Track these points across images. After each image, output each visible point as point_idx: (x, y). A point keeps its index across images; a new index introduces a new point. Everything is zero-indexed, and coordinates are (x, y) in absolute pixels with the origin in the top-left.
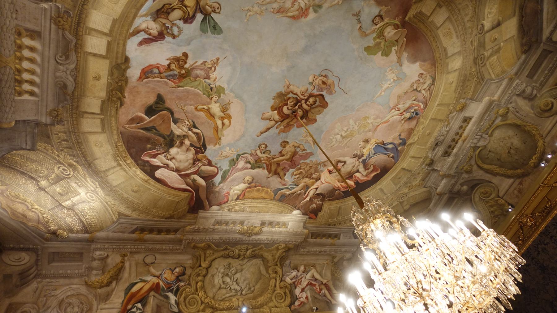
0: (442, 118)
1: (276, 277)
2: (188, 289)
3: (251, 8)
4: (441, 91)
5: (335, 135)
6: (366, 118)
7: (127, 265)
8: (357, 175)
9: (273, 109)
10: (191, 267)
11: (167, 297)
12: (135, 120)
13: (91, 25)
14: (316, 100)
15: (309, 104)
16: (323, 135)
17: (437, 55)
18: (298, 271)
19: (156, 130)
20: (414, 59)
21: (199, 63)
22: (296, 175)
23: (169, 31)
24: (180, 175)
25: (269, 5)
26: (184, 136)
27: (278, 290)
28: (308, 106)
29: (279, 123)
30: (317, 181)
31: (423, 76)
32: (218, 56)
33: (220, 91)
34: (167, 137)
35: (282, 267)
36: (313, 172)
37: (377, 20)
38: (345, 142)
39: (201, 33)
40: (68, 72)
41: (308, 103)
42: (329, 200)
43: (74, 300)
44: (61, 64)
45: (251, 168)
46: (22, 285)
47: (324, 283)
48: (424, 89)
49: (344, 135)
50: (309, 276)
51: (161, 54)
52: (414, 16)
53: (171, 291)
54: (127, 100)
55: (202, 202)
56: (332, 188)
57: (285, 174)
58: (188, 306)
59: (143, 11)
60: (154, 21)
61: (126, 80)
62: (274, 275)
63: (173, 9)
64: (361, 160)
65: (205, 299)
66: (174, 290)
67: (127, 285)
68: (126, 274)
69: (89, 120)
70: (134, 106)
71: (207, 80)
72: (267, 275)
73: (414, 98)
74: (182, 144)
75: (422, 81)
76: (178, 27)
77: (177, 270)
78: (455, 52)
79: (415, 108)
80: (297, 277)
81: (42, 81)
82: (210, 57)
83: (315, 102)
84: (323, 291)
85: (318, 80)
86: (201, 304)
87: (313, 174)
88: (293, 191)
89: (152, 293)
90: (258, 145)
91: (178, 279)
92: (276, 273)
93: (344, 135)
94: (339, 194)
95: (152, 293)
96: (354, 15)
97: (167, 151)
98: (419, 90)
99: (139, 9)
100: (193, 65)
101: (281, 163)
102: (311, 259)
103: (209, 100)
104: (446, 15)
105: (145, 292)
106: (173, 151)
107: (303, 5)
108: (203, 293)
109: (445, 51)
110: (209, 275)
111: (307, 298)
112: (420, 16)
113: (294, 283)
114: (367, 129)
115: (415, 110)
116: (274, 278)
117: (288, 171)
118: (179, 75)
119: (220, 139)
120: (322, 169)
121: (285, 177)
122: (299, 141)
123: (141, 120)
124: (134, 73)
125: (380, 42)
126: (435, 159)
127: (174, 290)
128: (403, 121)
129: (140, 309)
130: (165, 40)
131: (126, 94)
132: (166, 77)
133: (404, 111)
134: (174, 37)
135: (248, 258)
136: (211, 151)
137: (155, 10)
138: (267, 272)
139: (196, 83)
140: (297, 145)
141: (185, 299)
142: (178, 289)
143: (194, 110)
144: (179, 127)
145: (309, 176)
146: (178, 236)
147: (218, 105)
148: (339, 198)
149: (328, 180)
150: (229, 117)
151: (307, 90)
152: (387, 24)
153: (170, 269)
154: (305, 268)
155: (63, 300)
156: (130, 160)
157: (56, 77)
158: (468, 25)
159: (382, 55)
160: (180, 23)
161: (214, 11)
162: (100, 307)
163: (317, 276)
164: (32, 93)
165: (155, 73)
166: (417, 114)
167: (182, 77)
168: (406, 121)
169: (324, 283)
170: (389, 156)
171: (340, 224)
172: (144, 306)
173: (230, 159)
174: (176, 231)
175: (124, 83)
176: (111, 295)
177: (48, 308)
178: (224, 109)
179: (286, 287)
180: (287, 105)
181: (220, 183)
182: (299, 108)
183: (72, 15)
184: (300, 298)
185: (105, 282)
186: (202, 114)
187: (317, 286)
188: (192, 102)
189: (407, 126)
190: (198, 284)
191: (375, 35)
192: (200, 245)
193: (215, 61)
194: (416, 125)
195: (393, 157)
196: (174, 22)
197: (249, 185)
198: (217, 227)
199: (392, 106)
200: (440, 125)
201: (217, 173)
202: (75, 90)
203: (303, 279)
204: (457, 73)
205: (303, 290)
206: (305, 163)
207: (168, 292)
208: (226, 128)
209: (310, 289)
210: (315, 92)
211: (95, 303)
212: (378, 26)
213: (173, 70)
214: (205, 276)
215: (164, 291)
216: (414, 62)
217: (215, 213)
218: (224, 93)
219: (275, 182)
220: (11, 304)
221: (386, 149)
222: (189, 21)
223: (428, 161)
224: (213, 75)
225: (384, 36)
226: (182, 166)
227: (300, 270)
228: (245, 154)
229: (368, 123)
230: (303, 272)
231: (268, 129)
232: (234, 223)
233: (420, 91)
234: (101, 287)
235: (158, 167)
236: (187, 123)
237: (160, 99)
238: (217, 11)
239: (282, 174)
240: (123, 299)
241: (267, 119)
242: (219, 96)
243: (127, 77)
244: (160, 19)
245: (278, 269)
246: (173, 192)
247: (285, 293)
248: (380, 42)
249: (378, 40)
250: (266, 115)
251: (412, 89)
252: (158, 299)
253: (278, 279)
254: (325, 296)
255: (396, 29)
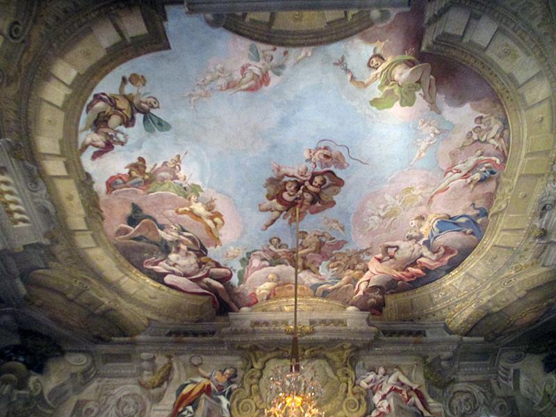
0: (541, 171)
1: (347, 380)
2: (241, 393)
3: (192, 93)
4: (526, 135)
5: (369, 216)
6: (408, 190)
7: (175, 365)
8: (422, 260)
9: (270, 198)
10: (242, 369)
11: (219, 401)
12: (122, 232)
13: (43, 150)
14: (325, 179)
15: (317, 184)
16: (351, 219)
17: (498, 87)
18: (377, 374)
19: (146, 239)
20: (459, 98)
21: (159, 165)
22: (333, 267)
23: (114, 139)
24: (191, 280)
25: (213, 83)
26: (177, 241)
27: (350, 397)
28: (317, 187)
29: (285, 212)
30: (365, 272)
31: (483, 121)
32: (177, 153)
33: (196, 189)
34: (160, 244)
35: (354, 369)
36: (355, 262)
37: (375, 62)
38: (389, 222)
39: (147, 133)
40: (44, 197)
41: (314, 183)
42: (392, 293)
43: (130, 400)
44: (36, 191)
45: (271, 265)
46: (86, 383)
47: (414, 388)
48: (493, 138)
49: (382, 214)
50: (392, 380)
51: (116, 163)
52: (434, 43)
53: (223, 394)
54: (105, 214)
55: (227, 305)
56: (390, 279)
57: (318, 268)
58: (241, 411)
59: (82, 125)
60: (96, 132)
61: (96, 195)
62: (345, 378)
63: (109, 117)
64: (421, 242)
65: (260, 404)
66: (226, 393)
67: (177, 387)
68: (175, 375)
69: (81, 237)
70: (115, 219)
71: (176, 181)
72: (336, 378)
73: (479, 152)
74: (178, 249)
75: (483, 127)
76: (122, 133)
77: (228, 371)
78: (531, 75)
79: (486, 165)
80: (376, 381)
81: (27, 209)
82: (168, 155)
83: (324, 182)
84: (412, 399)
85: (317, 154)
86: (256, 410)
87: (356, 262)
88: (336, 285)
89: (203, 395)
90: (268, 240)
91: (230, 381)
92: (347, 375)
93: (382, 214)
94: (403, 284)
95: (203, 395)
96: (335, 64)
97: (166, 258)
98: (483, 139)
99: (77, 125)
100: (153, 169)
101: (307, 256)
102: (394, 360)
103: (187, 201)
104: (493, 27)
105: (196, 395)
106: (173, 257)
107: (257, 71)
108: (258, 397)
109: (511, 77)
110: (265, 377)
111: (389, 407)
112: (445, 40)
113: (372, 388)
114: (416, 203)
115: (486, 168)
116: (345, 382)
117: (320, 264)
118: (145, 182)
119: (218, 239)
120: (366, 258)
121: (320, 271)
122: (321, 229)
123: (127, 231)
124: (100, 186)
125: (393, 90)
126: (549, 228)
127: (226, 393)
128: (472, 186)
129: (191, 413)
130: (115, 149)
131: (102, 209)
132: (133, 185)
133: (469, 172)
134: (123, 144)
135: (307, 358)
136: (212, 252)
137: (92, 121)
138: (335, 374)
139: (166, 186)
140: (320, 234)
141: (238, 403)
142: (230, 392)
143: (176, 214)
144: (167, 233)
145: (352, 267)
146: (216, 338)
147: (200, 204)
148: (403, 289)
149: (380, 270)
150: (219, 215)
151: (307, 169)
152: (392, 63)
153: (220, 370)
154: (386, 370)
155: (120, 400)
156: (135, 270)
157: (35, 203)
158: (542, 30)
159: (402, 105)
160: (122, 128)
161: (152, 107)
162: (153, 408)
163: (404, 380)
164: (24, 221)
165: (120, 184)
166: (492, 173)
167: (147, 182)
168: (476, 184)
169: (414, 388)
170: (465, 232)
171: (419, 318)
172: (195, 409)
173: (239, 258)
174: (213, 333)
175: (95, 198)
176: (163, 397)
177: (108, 407)
178: (210, 207)
179: (361, 393)
180: (286, 190)
181: (239, 284)
182: (303, 191)
183: (23, 146)
184: (379, 407)
185: (157, 382)
186: (185, 216)
187: (404, 393)
188: (170, 206)
189: (480, 190)
190: (253, 387)
191: (379, 82)
192: (245, 346)
193: (176, 159)
194: (496, 188)
195: (472, 233)
196: (116, 129)
197: (276, 284)
198: (256, 328)
199: (445, 169)
200: (540, 184)
201: (231, 275)
202: (56, 213)
203: (385, 383)
204: (546, 105)
205: (384, 397)
206: (340, 253)
207: (220, 395)
208: (220, 228)
209: (394, 396)
210: (319, 169)
211: (148, 403)
212: (380, 70)
213: (136, 177)
214: (259, 378)
215: (216, 394)
216: (462, 104)
217: (246, 316)
218: (202, 191)
219: (307, 278)
220: (78, 402)
221: (456, 224)
222: (131, 124)
223: (537, 232)
224: (181, 174)
225: (394, 80)
226: (189, 270)
227: (379, 373)
228: (255, 251)
229: (414, 195)
230: (384, 375)
231: (273, 221)
232: (276, 323)
233: (486, 142)
234: (153, 388)
235: (165, 274)
236: (174, 227)
237: (136, 208)
238: (155, 106)
239: (313, 268)
240: (175, 400)
241: (267, 210)
242: (198, 195)
243: (95, 192)
244: (102, 130)
245: (349, 370)
246: (190, 296)
247: (360, 401)
248: (393, 90)
249: (387, 88)
250: (264, 207)
251: (472, 141)
252: (209, 402)
253: (350, 382)
254: (415, 405)
255: (411, 67)
